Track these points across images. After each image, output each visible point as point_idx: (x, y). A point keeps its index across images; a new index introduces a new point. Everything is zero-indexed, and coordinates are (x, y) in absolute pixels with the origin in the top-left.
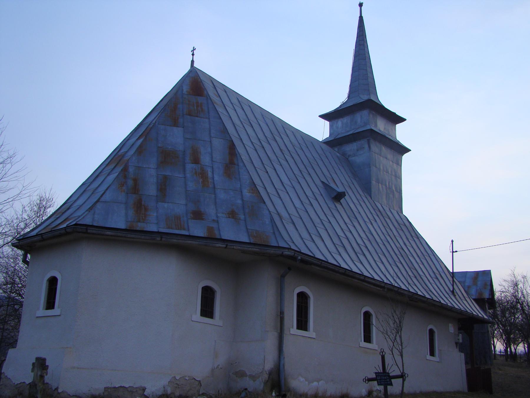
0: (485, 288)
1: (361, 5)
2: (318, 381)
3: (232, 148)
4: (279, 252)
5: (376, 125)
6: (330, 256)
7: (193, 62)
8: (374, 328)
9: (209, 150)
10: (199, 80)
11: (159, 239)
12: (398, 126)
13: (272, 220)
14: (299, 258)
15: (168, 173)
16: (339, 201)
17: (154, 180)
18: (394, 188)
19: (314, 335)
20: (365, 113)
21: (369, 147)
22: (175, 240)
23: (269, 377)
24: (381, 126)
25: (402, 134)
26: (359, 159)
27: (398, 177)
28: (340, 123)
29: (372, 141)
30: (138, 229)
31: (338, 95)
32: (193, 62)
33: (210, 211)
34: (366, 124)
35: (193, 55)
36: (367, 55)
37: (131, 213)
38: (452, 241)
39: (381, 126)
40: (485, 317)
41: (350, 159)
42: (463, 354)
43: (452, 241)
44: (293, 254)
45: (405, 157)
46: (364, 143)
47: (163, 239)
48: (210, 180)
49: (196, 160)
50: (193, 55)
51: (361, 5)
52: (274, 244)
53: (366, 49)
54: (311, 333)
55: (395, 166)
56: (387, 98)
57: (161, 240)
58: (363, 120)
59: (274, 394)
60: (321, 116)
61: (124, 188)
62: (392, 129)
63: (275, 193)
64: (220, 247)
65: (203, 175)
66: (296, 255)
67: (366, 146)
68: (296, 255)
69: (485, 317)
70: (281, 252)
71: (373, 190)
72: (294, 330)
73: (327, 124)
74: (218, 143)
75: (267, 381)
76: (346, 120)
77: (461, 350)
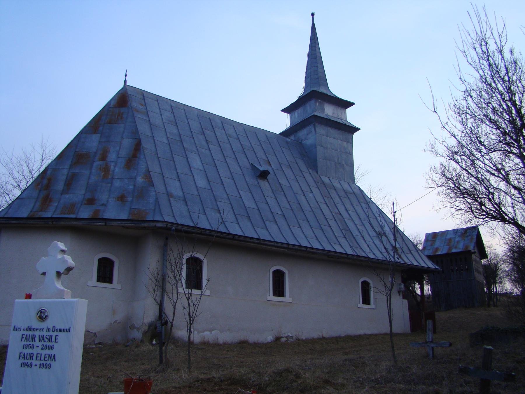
0: (471, 242)
1: (313, 15)
2: (211, 330)
3: (138, 147)
4: (152, 225)
5: (323, 111)
6: (355, 228)
7: (125, 81)
8: (372, 289)
9: (118, 148)
10: (127, 95)
11: (50, 223)
12: (348, 110)
13: (157, 201)
14: (174, 228)
15: (77, 171)
16: (266, 178)
17: (64, 177)
18: (344, 163)
19: (290, 300)
20: (313, 102)
21: (315, 130)
22: (62, 223)
23: (149, 329)
24: (329, 111)
25: (351, 116)
26: (309, 142)
27: (350, 154)
28: (296, 114)
29: (317, 124)
30: (37, 216)
31: (296, 89)
32: (125, 81)
33: (103, 197)
34: (313, 112)
35: (126, 76)
36: (318, 54)
37: (38, 204)
38: (393, 203)
39: (329, 111)
40: (437, 267)
41: (303, 142)
42: (406, 301)
43: (393, 203)
44: (165, 226)
45: (356, 136)
46: (311, 127)
47: (54, 223)
48: (111, 173)
49: (104, 158)
50: (126, 76)
51: (313, 15)
52: (150, 218)
53: (317, 50)
54: (287, 298)
55: (345, 144)
56: (337, 87)
57: (53, 224)
58: (313, 108)
59: (154, 342)
60: (353, 104)
61: (39, 187)
62: (342, 113)
63: (293, 177)
64: (100, 225)
65: (106, 170)
66: (168, 226)
67: (313, 130)
68: (168, 226)
69: (437, 267)
70: (154, 225)
71: (319, 166)
72: (182, 289)
73: (287, 116)
74: (127, 143)
75: (147, 332)
76: (300, 110)
77: (404, 298)
